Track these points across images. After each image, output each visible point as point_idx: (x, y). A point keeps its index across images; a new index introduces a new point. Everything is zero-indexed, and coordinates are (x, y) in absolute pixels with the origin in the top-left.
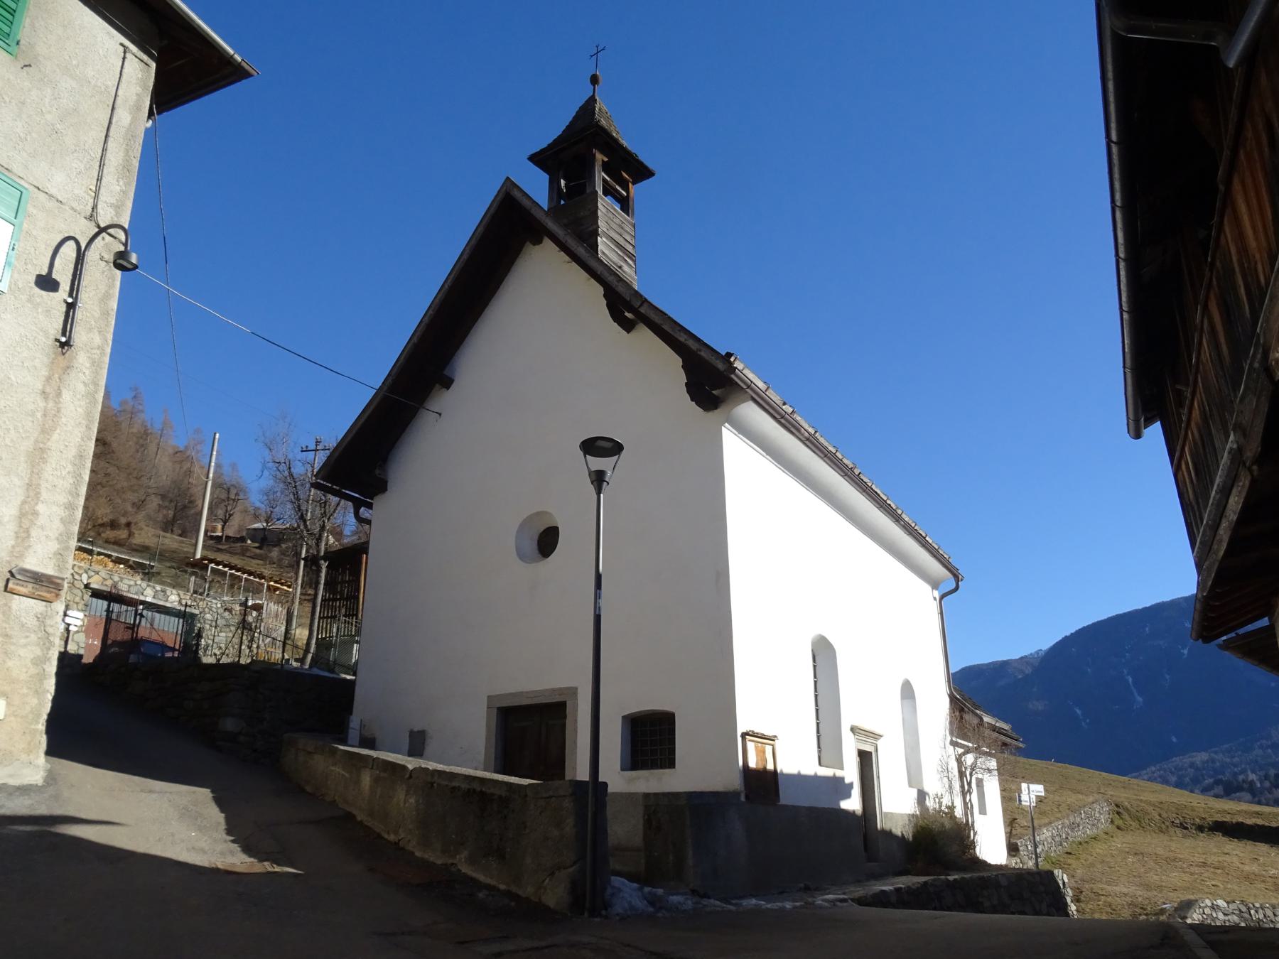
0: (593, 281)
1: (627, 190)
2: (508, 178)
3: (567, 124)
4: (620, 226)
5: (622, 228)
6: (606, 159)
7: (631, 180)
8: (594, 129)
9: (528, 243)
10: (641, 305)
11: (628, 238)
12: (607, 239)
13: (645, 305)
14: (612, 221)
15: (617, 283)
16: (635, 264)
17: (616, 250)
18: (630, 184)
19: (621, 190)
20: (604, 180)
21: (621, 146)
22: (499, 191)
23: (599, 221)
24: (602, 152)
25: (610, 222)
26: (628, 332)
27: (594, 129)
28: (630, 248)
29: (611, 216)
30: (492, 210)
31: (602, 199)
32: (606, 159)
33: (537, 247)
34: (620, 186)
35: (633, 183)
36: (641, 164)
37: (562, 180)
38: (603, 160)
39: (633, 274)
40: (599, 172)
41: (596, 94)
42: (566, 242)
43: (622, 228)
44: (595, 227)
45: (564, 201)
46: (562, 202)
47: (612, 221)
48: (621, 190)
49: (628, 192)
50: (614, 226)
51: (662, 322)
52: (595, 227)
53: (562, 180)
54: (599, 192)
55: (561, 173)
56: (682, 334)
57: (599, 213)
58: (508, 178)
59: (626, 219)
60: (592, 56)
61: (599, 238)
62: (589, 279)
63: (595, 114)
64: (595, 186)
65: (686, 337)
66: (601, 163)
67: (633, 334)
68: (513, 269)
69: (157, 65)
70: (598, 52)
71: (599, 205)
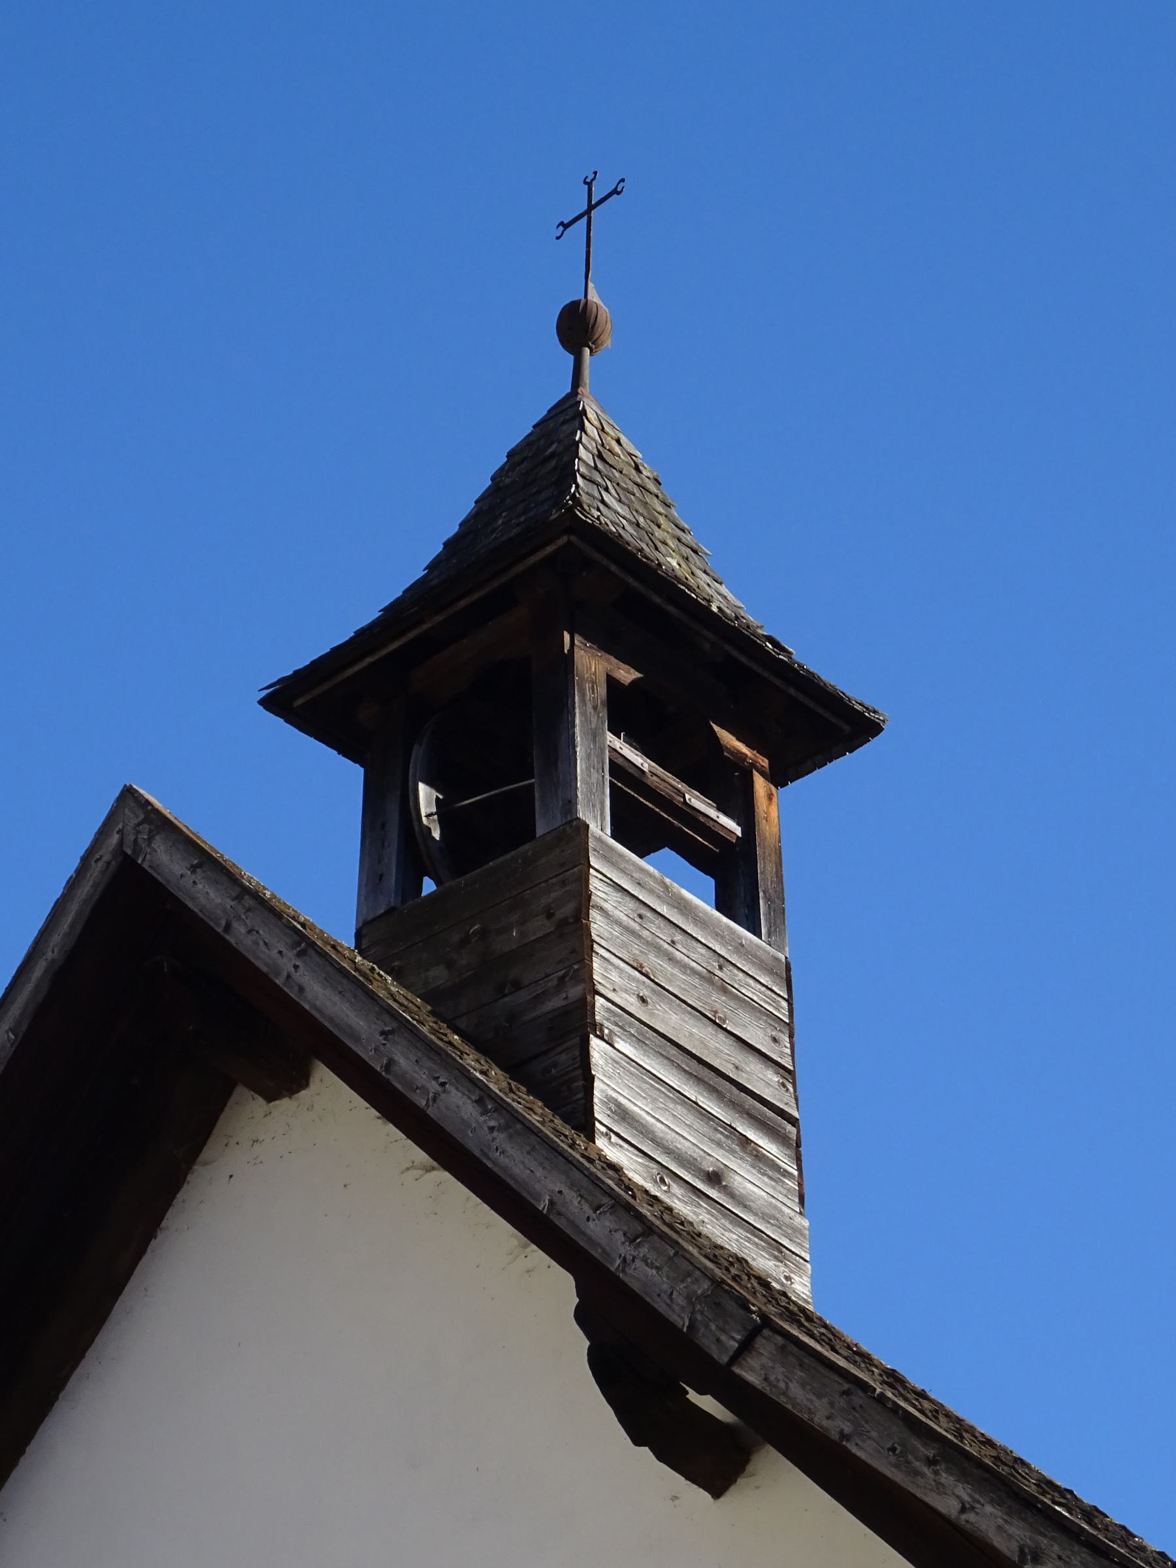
0: (538, 1257)
1: (746, 813)
2: (128, 793)
3: (452, 529)
4: (709, 978)
5: (724, 988)
6: (627, 675)
7: (764, 762)
8: (563, 540)
9: (241, 1093)
10: (746, 1347)
11: (757, 1036)
12: (639, 1042)
13: (766, 1347)
14: (671, 959)
15: (626, 1250)
16: (796, 1149)
17: (691, 1092)
18: (760, 785)
19: (713, 813)
20: (620, 770)
21: (699, 611)
22: (86, 859)
23: (596, 964)
24: (607, 643)
25: (652, 961)
26: (717, 1492)
27: (563, 540)
28: (765, 1081)
29: (664, 934)
30: (53, 952)
31: (609, 857)
32: (627, 675)
33: (285, 1104)
34: (706, 792)
35: (779, 778)
36: (808, 684)
37: (422, 788)
38: (612, 682)
39: (789, 1208)
40: (594, 736)
41: (585, 391)
42: (388, 1066)
43: (724, 988)
44: (574, 992)
45: (438, 882)
46: (429, 886)
47: (671, 959)
48: (713, 813)
49: (747, 816)
50: (678, 982)
51: (847, 1428)
52: (574, 992)
53: (422, 788)
54: (594, 828)
55: (418, 753)
56: (946, 1478)
57: (598, 925)
58: (128, 793)
59: (740, 948)
60: (566, 226)
61: (595, 1042)
62: (525, 1247)
63: (570, 475)
64: (570, 805)
65: (964, 1492)
66: (602, 691)
67: (739, 1497)
68: (172, 1220)
69: (575, 357)
70: (591, 207)
71: (596, 885)
